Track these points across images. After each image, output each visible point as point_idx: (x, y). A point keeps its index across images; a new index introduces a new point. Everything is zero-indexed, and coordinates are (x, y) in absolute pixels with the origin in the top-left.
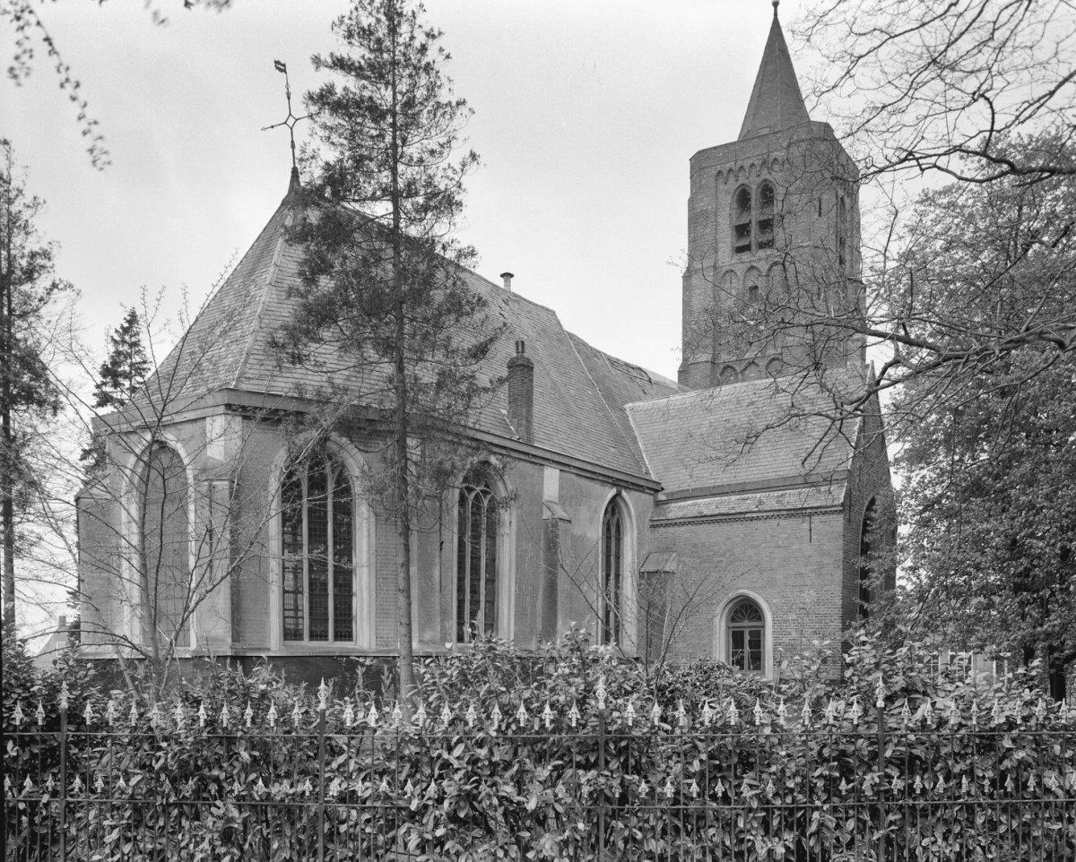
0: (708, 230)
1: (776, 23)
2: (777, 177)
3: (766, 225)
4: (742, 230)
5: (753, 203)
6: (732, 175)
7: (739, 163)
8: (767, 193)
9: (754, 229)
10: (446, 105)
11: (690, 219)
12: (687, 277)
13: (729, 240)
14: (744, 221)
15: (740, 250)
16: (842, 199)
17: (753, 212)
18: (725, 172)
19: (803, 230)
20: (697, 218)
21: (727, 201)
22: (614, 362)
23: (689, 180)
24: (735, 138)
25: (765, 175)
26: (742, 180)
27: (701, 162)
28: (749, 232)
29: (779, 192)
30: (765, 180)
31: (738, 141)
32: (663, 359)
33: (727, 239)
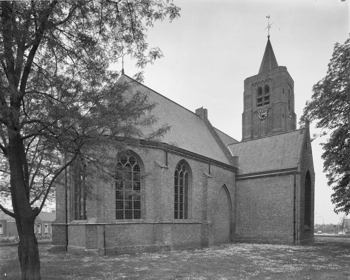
0: (249, 101)
1: (269, 41)
2: (270, 84)
3: (267, 98)
4: (260, 100)
5: (263, 92)
6: (256, 84)
7: (259, 81)
8: (267, 89)
9: (263, 99)
10: (330, 66)
11: (244, 98)
12: (243, 115)
13: (256, 103)
14: (260, 97)
16: (289, 90)
17: (263, 95)
18: (254, 84)
19: (276, 96)
20: (246, 97)
21: (255, 92)
22: (259, 72)
23: (244, 87)
24: (257, 74)
25: (267, 83)
26: (259, 85)
27: (247, 81)
28: (262, 100)
29: (271, 90)
30: (266, 85)
31: (259, 74)
32: (238, 136)
33: (255, 102)
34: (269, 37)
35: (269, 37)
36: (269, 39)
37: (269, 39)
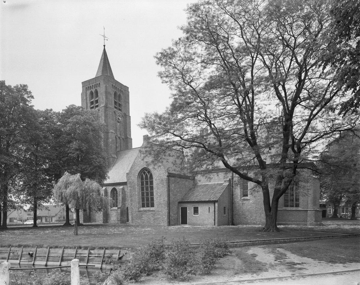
1: (104, 49)
4: (115, 103)
15: (115, 107)
34: (104, 46)
35: (104, 46)
36: (104, 47)
37: (104, 47)
